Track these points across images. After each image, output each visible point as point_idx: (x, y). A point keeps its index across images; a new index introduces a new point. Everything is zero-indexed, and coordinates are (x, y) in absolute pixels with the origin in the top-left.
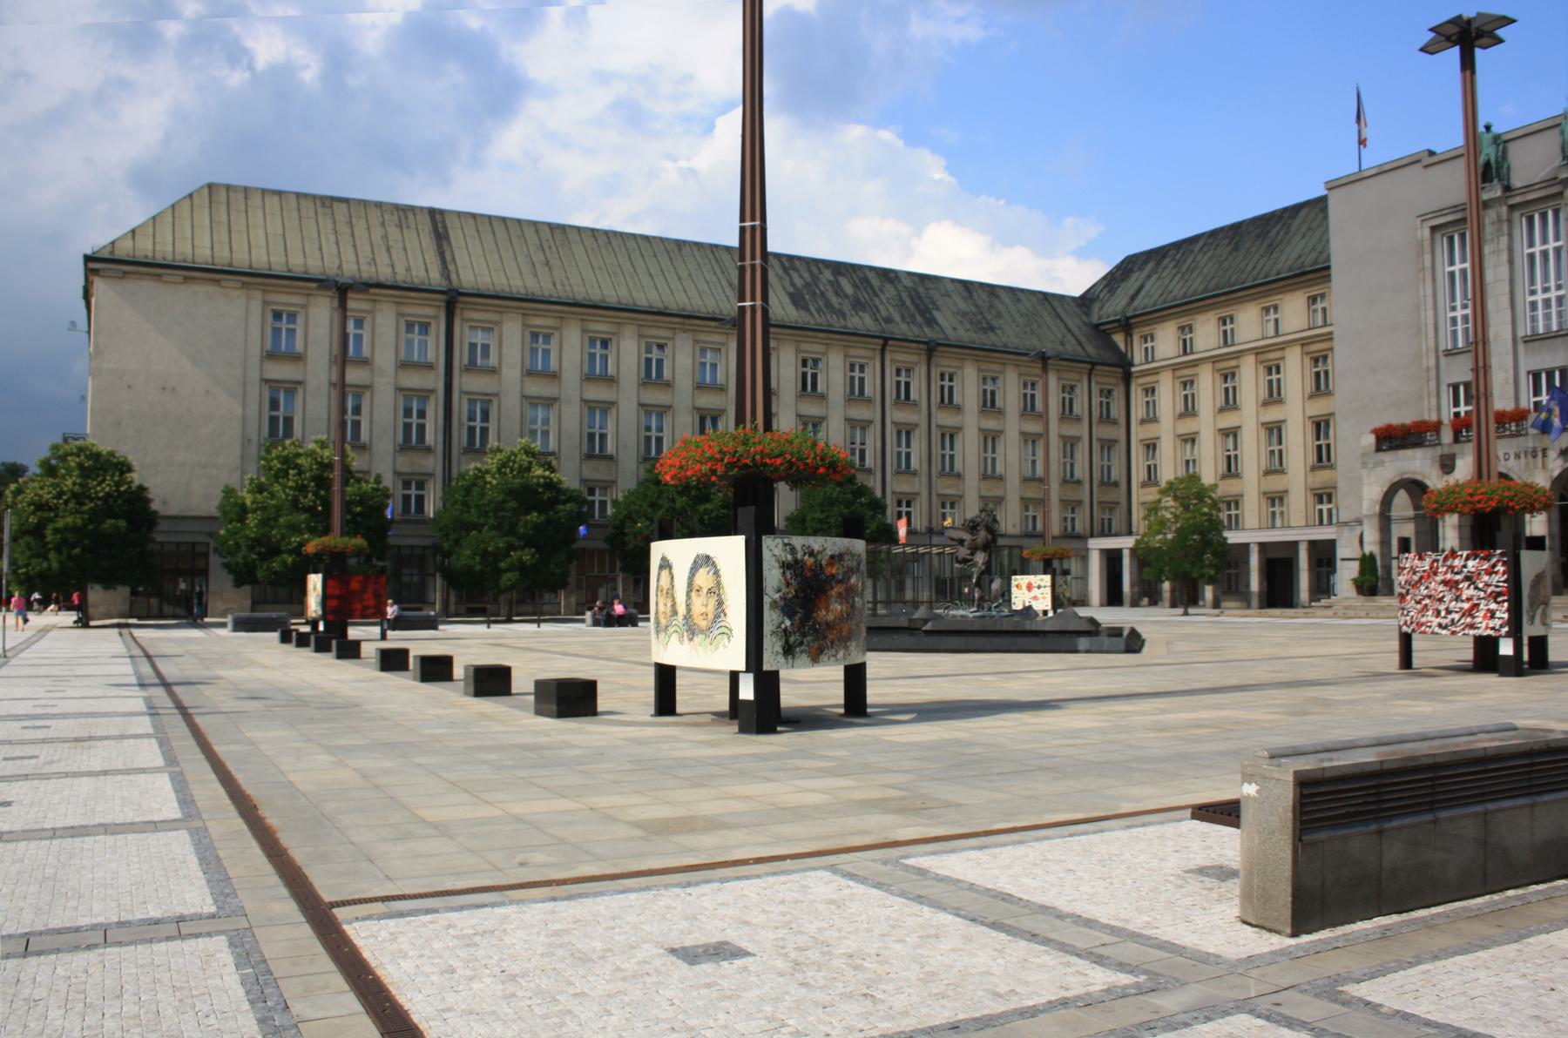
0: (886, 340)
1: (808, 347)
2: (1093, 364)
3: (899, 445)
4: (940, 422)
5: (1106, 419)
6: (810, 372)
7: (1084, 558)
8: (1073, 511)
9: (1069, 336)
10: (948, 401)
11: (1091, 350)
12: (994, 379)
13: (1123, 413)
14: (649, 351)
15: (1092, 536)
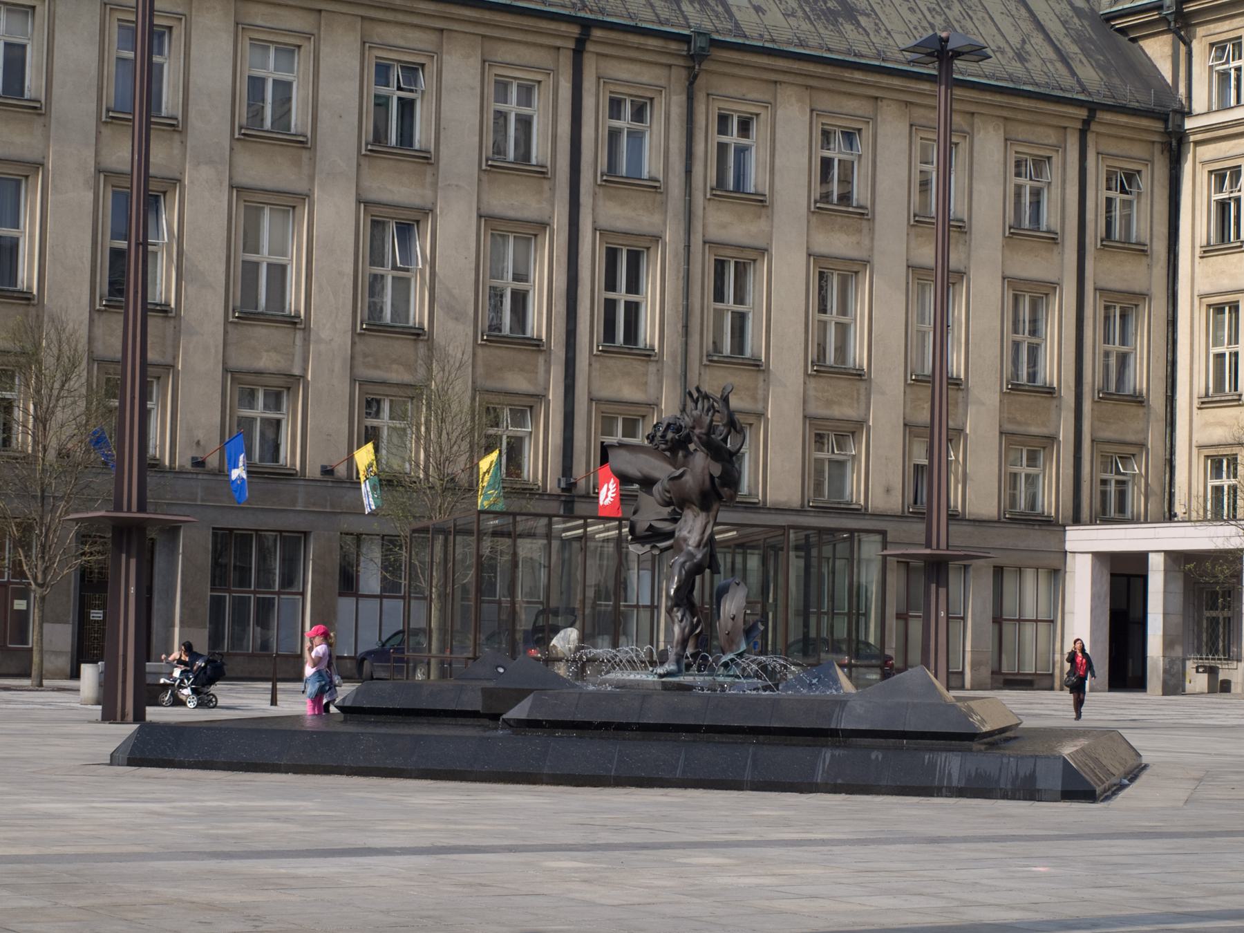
0: (587, 26)
1: (392, 35)
2: (1093, 108)
3: (611, 285)
4: (715, 234)
5: (1119, 243)
6: (1027, 184)
7: (1056, 574)
8: (1032, 460)
9: (1037, 39)
10: (732, 188)
11: (1089, 74)
12: (849, 136)
13: (1162, 229)
14: (502, 96)
15: (1077, 520)
